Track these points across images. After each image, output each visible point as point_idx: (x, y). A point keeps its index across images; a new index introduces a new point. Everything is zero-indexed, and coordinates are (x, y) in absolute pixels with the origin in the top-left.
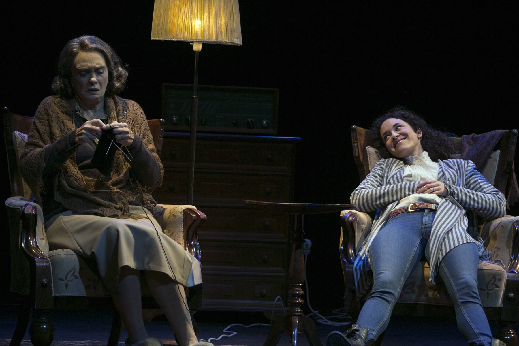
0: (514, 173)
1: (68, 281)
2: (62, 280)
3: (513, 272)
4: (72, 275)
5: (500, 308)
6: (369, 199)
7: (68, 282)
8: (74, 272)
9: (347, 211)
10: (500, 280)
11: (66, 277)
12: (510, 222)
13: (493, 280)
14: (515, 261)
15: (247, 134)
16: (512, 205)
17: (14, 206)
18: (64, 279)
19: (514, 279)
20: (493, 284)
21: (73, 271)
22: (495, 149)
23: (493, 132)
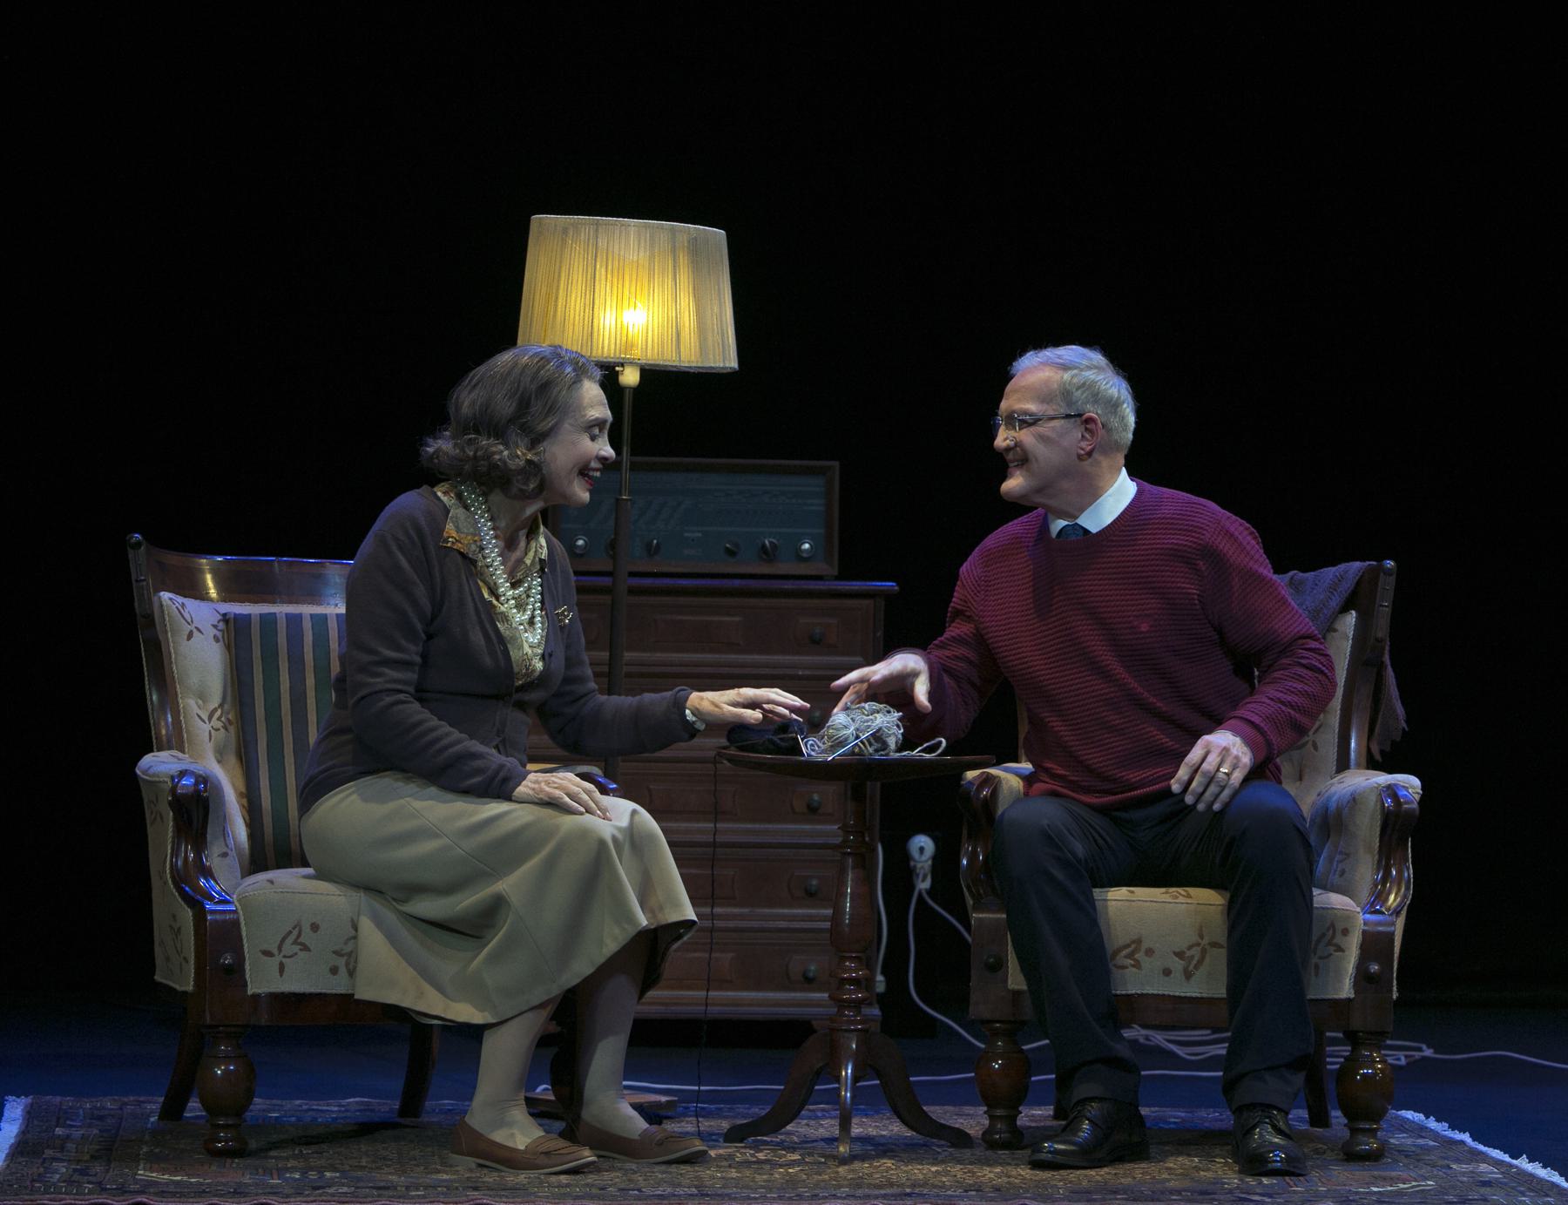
0: (1390, 669)
2: (268, 954)
4: (295, 942)
5: (1349, 1000)
6: (438, 746)
8: (299, 935)
9: (976, 773)
10: (1345, 932)
11: (280, 949)
12: (1372, 789)
14: (1384, 885)
15: (763, 577)
16: (1388, 749)
17: (154, 775)
18: (275, 951)
21: (295, 933)
22: (1345, 609)
23: (1343, 566)
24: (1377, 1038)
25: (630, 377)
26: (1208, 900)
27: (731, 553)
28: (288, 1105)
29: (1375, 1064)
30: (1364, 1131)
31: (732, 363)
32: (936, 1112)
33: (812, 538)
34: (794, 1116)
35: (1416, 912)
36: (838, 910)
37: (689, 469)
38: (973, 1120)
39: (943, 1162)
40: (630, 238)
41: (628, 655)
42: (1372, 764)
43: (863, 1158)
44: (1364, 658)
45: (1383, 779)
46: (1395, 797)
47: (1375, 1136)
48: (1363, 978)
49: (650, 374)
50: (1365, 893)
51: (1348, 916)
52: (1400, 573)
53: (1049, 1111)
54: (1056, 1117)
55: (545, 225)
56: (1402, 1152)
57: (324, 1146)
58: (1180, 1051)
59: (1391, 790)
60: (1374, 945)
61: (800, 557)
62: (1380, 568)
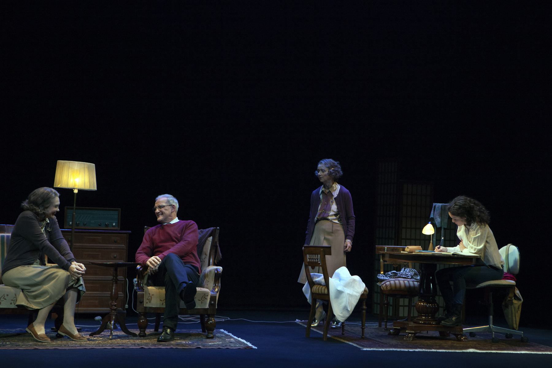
0: (219, 248)
22: (210, 236)
24: (213, 316)
25: (76, 191)
26: (163, 291)
28: (5, 330)
29: (212, 321)
31: (95, 189)
32: (130, 330)
33: (116, 223)
34: (103, 331)
35: (221, 292)
36: (112, 292)
37: (96, 210)
38: (137, 332)
40: (76, 165)
41: (74, 244)
42: (215, 264)
43: (114, 339)
44: (214, 246)
45: (216, 267)
46: (217, 271)
48: (210, 304)
49: (80, 191)
50: (211, 289)
53: (153, 330)
55: (60, 163)
56: (218, 337)
58: (182, 319)
59: (217, 269)
60: (213, 298)
61: (113, 226)
62: (216, 229)
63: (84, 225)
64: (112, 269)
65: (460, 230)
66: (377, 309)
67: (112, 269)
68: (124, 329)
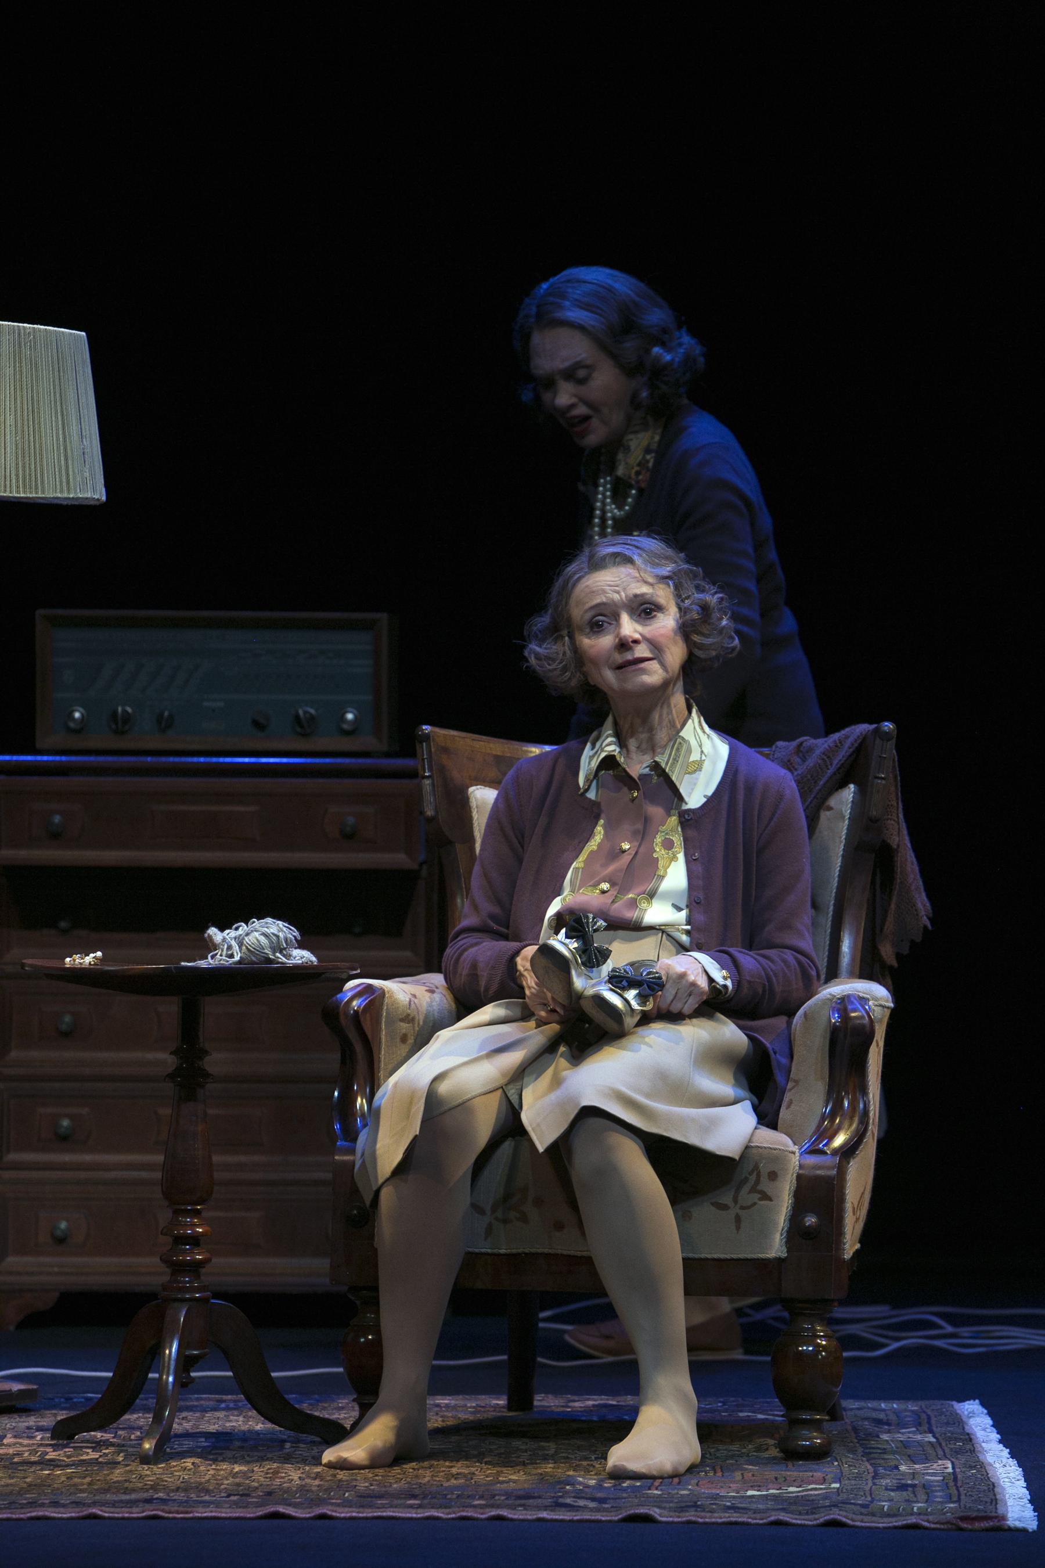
1: (742, 1208)
3: (822, 1152)
5: (779, 1260)
7: (741, 1213)
10: (773, 1176)
13: (754, 1177)
14: (832, 1120)
16: (906, 951)
18: (730, 1203)
19: (819, 1172)
20: (753, 1190)
22: (842, 785)
27: (259, 726)
30: (805, 1422)
39: (248, 1462)
44: (870, 854)
47: (820, 1430)
48: (796, 1232)
51: (777, 1157)
52: (903, 741)
54: (510, 1407)
57: (517, 1443)
60: (819, 1195)
63: (164, 724)
64: (169, 1008)
65: (664, 627)
66: (305, 1270)
67: (169, 1008)
68: (267, 1400)
